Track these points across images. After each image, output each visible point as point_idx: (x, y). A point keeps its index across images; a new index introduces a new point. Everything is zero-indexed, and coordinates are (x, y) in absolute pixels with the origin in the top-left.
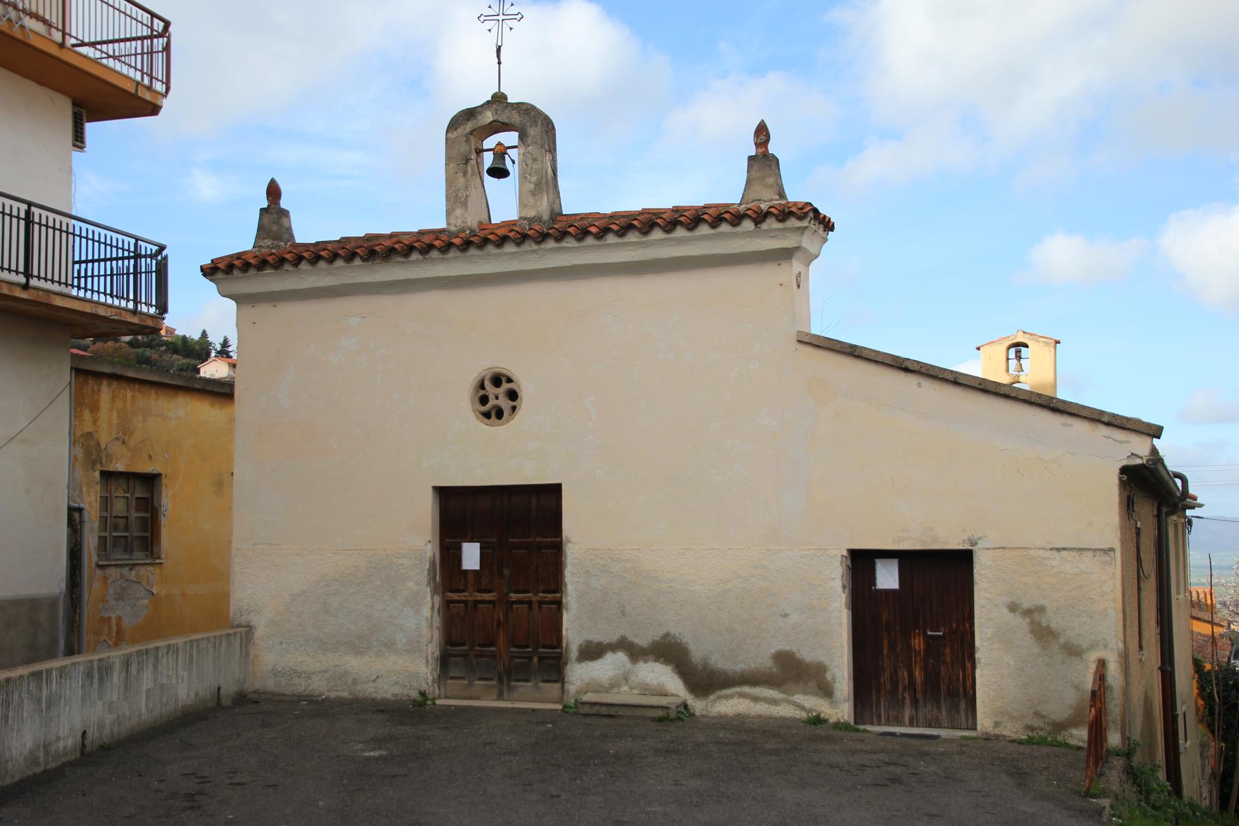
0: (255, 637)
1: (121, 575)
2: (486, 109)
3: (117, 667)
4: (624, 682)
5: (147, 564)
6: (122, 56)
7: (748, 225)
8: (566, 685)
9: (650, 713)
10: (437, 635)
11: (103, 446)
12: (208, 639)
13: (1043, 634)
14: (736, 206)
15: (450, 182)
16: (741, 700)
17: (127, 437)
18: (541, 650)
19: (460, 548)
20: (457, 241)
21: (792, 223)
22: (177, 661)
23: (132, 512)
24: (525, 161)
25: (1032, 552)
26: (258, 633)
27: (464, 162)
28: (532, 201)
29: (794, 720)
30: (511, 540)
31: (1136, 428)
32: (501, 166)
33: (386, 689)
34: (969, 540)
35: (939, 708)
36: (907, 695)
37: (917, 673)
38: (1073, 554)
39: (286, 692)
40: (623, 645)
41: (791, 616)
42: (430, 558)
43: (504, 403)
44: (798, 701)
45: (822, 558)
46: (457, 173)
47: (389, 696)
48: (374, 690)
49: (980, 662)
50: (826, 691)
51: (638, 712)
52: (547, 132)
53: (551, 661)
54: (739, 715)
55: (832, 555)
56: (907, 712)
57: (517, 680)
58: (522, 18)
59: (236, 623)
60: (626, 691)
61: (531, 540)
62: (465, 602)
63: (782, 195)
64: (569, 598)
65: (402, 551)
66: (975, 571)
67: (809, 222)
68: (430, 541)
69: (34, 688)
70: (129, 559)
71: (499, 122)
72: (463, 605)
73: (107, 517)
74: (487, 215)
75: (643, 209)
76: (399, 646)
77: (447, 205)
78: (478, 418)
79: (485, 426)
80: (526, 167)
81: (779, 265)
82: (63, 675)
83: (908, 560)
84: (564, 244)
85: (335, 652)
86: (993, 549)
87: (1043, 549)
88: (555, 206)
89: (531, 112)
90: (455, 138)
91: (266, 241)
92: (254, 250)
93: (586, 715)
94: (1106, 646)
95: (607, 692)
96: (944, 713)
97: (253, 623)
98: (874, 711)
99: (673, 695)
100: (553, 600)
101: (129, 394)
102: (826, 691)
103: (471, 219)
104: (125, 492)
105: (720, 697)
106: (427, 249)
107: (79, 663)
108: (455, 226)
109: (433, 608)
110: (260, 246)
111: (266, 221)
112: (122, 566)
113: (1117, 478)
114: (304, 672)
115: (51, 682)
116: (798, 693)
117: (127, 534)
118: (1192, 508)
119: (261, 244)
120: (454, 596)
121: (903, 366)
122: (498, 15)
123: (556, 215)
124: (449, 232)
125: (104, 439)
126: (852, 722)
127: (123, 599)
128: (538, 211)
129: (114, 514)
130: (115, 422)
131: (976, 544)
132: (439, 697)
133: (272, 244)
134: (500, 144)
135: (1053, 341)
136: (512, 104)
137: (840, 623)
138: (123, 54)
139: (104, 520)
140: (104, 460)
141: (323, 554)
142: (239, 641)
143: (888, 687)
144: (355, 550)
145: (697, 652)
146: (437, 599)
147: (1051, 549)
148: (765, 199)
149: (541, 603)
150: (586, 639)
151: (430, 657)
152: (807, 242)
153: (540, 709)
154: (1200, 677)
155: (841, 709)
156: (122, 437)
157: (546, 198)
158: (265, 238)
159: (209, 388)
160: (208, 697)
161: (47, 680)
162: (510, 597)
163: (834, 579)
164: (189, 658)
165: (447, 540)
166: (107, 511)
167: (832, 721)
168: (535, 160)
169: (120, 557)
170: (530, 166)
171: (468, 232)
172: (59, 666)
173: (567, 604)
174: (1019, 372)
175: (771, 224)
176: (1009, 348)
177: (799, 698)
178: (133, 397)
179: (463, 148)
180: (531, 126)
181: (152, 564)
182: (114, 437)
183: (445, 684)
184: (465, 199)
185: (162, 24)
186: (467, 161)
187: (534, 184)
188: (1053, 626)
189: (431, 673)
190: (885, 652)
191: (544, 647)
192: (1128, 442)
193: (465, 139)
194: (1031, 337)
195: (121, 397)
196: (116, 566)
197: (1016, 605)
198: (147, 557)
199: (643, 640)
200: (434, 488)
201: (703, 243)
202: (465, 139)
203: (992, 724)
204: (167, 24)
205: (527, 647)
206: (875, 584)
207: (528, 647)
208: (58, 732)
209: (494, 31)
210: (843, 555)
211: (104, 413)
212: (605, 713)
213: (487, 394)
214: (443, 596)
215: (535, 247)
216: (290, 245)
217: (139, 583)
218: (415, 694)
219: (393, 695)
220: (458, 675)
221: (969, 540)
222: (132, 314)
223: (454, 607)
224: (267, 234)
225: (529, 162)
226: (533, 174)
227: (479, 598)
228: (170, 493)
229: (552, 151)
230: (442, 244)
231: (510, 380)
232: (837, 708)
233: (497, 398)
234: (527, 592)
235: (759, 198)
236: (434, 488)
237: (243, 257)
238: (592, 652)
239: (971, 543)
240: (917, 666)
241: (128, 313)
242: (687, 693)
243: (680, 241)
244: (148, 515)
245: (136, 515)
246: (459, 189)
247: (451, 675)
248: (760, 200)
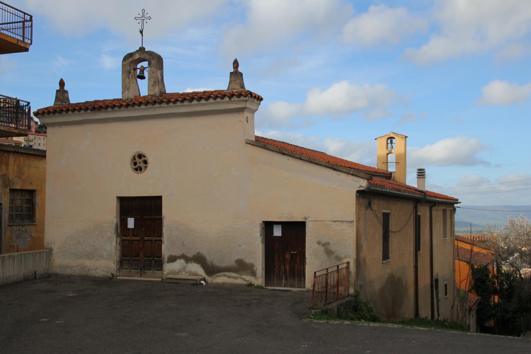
0: (53, 253)
4: (183, 270)
5: (30, 225)
6: (8, 29)
7: (227, 99)
9: (191, 282)
10: (118, 253)
11: (11, 179)
12: (30, 253)
13: (329, 252)
14: (225, 91)
15: (123, 81)
16: (224, 277)
18: (155, 258)
19: (127, 220)
20: (124, 104)
21: (242, 98)
22: (14, 261)
23: (24, 205)
24: (150, 73)
25: (326, 222)
26: (54, 252)
29: (242, 285)
30: (145, 217)
31: (361, 176)
32: (143, 75)
33: (100, 273)
34: (304, 218)
35: (295, 280)
36: (283, 275)
37: (287, 267)
38: (340, 223)
39: (64, 274)
41: (242, 246)
42: (115, 223)
43: (142, 165)
44: (244, 278)
46: (126, 77)
47: (101, 275)
48: (95, 273)
49: (307, 263)
50: (254, 274)
51: (186, 282)
52: (158, 62)
54: (223, 283)
56: (284, 282)
58: (135, 18)
59: (46, 248)
60: (184, 274)
62: (129, 240)
63: (242, 86)
64: (164, 239)
66: (306, 229)
67: (249, 98)
70: (22, 223)
72: (128, 241)
73: (13, 207)
74: (139, 93)
75: (193, 92)
77: (122, 90)
78: (133, 171)
79: (135, 174)
81: (239, 114)
83: (285, 225)
84: (162, 105)
85: (82, 259)
86: (313, 221)
87: (329, 221)
88: (162, 90)
90: (125, 64)
91: (58, 102)
93: (168, 283)
94: (350, 257)
95: (177, 274)
96: (296, 282)
98: (272, 281)
99: (200, 276)
101: (22, 159)
102: (254, 274)
103: (131, 95)
104: (21, 197)
105: (217, 276)
106: (113, 107)
108: (125, 98)
109: (116, 242)
110: (56, 104)
111: (58, 95)
112: (19, 225)
113: (355, 195)
116: (244, 275)
117: (22, 213)
118: (457, 203)
119: (56, 104)
120: (125, 238)
121: (282, 152)
122: (142, 17)
123: (163, 93)
124: (123, 100)
125: (11, 177)
126: (264, 285)
128: (154, 93)
129: (16, 205)
131: (307, 219)
132: (119, 276)
133: (61, 104)
134: (142, 66)
135: (404, 137)
137: (259, 249)
138: (19, 27)
139: (11, 209)
140: (11, 185)
143: (277, 272)
144: (89, 220)
145: (209, 259)
146: (119, 239)
147: (332, 221)
148: (236, 89)
149: (156, 241)
150: (170, 254)
151: (115, 261)
152: (248, 105)
153: (153, 281)
154: (473, 270)
155: (259, 280)
158: (58, 101)
162: (145, 239)
163: (258, 232)
165: (123, 217)
166: (13, 204)
167: (256, 285)
168: (154, 73)
169: (19, 222)
170: (152, 75)
171: (129, 100)
174: (392, 149)
175: (235, 98)
176: (388, 139)
177: (244, 277)
179: (128, 68)
181: (32, 225)
182: (15, 175)
184: (129, 88)
185: (30, 17)
186: (130, 73)
187: (153, 82)
188: (332, 250)
190: (276, 259)
192: (359, 181)
193: (129, 64)
194: (396, 135)
197: (320, 242)
199: (190, 255)
201: (211, 106)
203: (311, 286)
204: (31, 17)
205: (150, 257)
206: (273, 234)
209: (141, 23)
210: (260, 224)
211: (11, 166)
212: (175, 282)
215: (152, 106)
216: (67, 104)
218: (110, 275)
219: (102, 275)
220: (126, 267)
221: (304, 218)
222: (15, 129)
223: (125, 242)
225: (152, 74)
226: (153, 78)
227: (134, 239)
229: (161, 69)
231: (144, 157)
232: (257, 280)
233: (140, 163)
234: (150, 236)
235: (234, 88)
236: (118, 197)
238: (172, 259)
239: (305, 219)
240: (287, 265)
242: (205, 275)
243: (203, 105)
244: (31, 206)
245: (26, 206)
246: (127, 84)
247: (124, 268)
248: (234, 89)
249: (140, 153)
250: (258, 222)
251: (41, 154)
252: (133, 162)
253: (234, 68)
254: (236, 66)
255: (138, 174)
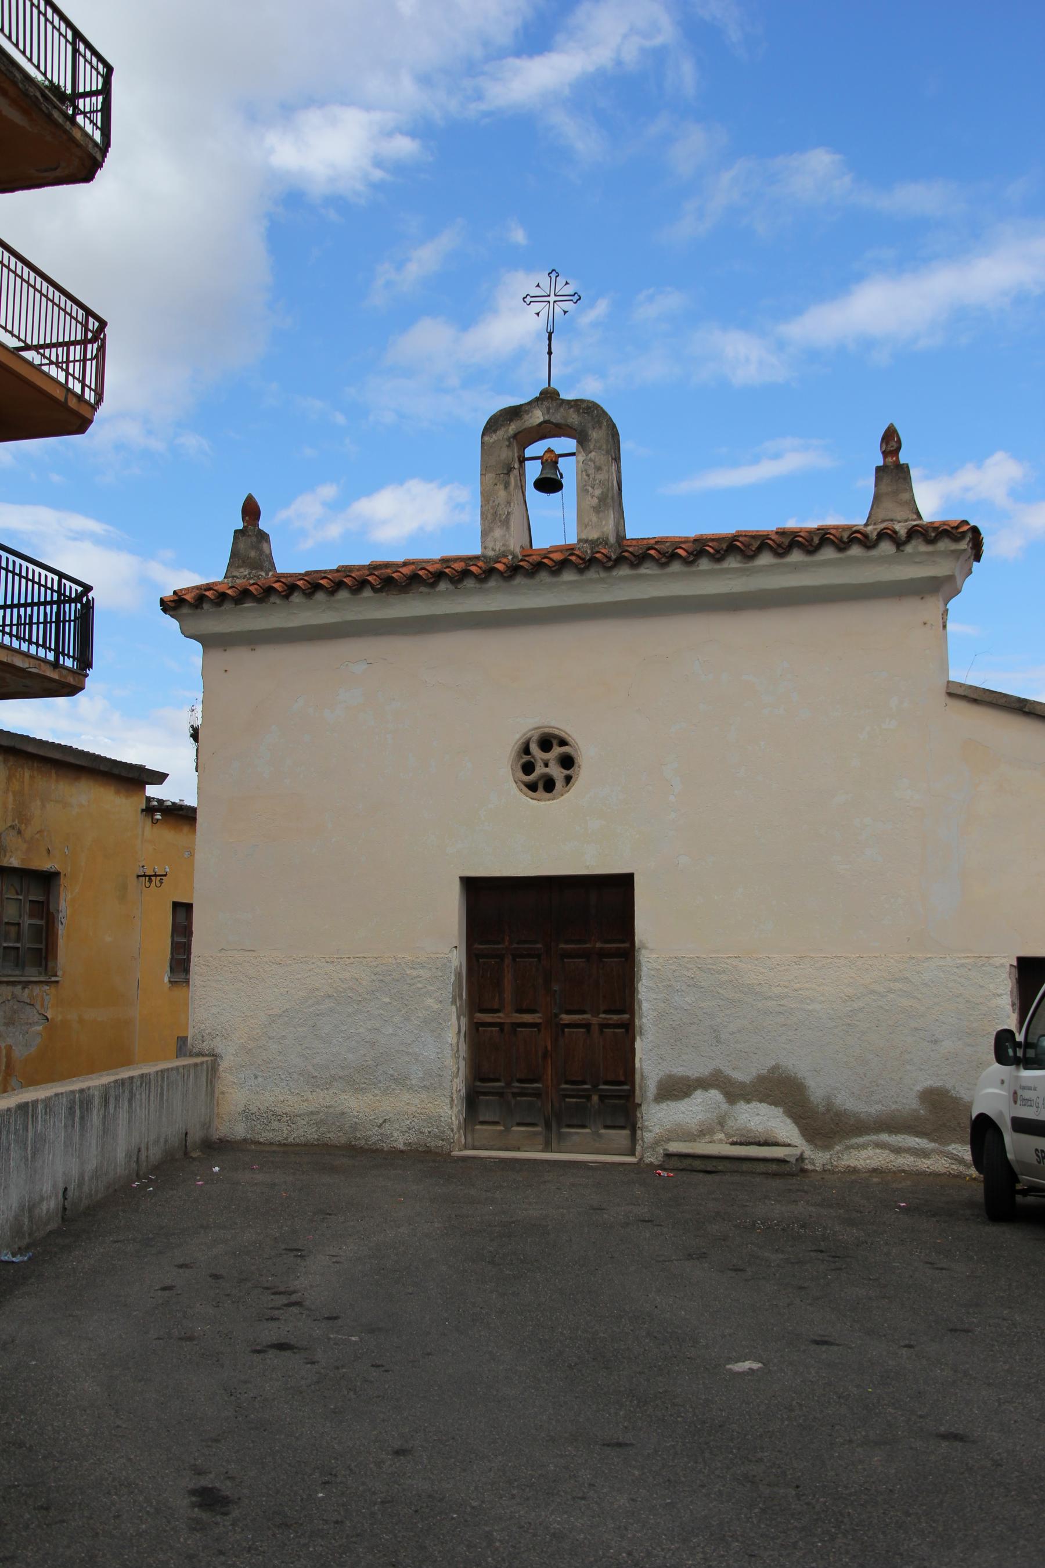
0: (221, 1069)
1: (13, 994)
2: (535, 407)
3: (96, 1102)
4: (719, 1128)
8: (639, 1132)
9: (761, 1167)
17: (23, 825)
22: (149, 1097)
24: (586, 470)
26: (224, 1065)
27: (505, 472)
28: (594, 519)
39: (261, 1140)
40: (716, 1081)
41: (943, 1043)
44: (954, 1152)
45: (984, 968)
53: (616, 1101)
55: (997, 964)
57: (569, 1126)
58: (580, 299)
60: (721, 1140)
61: (588, 945)
62: (500, 1025)
64: (644, 1020)
65: (419, 961)
68: (456, 947)
69: (21, 1126)
70: (22, 976)
71: (552, 423)
74: (528, 540)
75: (738, 532)
76: (413, 1082)
78: (521, 790)
80: (586, 478)
82: (48, 1110)
84: (643, 571)
89: (593, 411)
90: (493, 443)
91: (242, 570)
92: (226, 580)
97: (218, 1051)
100: (619, 1022)
101: (27, 774)
103: (515, 544)
105: (848, 1148)
107: (62, 1093)
110: (233, 577)
111: (241, 546)
114: (286, 1114)
115: (37, 1118)
116: (953, 1142)
117: (19, 945)
119: (235, 573)
120: (487, 1018)
122: (549, 296)
127: (14, 1024)
130: (10, 807)
133: (249, 574)
134: (550, 451)
136: (568, 402)
141: (313, 963)
142: (205, 1073)
144: (354, 958)
145: (818, 1089)
146: (464, 1020)
148: (899, 519)
156: (18, 825)
157: (612, 516)
158: (239, 567)
159: (116, 771)
160: (176, 1145)
161: (33, 1116)
162: (561, 1019)
163: (1001, 995)
164: (160, 1094)
165: (476, 946)
168: (598, 469)
169: (10, 972)
170: (592, 476)
172: (43, 1097)
173: (640, 1027)
178: (32, 777)
180: (594, 428)
181: (47, 983)
183: (473, 1130)
185: (97, 324)
189: (456, 1117)
191: (606, 1083)
193: (507, 443)
195: (18, 777)
196: (8, 983)
198: (40, 974)
199: (743, 1074)
200: (461, 879)
202: (507, 443)
204: (103, 324)
207: (584, 1083)
208: (42, 1190)
210: (1011, 965)
213: (532, 760)
214: (471, 1018)
217: (33, 1005)
220: (487, 1118)
224: (244, 562)
225: (591, 471)
228: (69, 897)
230: (479, 571)
231: (563, 743)
233: (546, 765)
234: (584, 1012)
236: (461, 879)
237: (216, 588)
241: (48, 666)
243: (796, 568)
244: (42, 922)
247: (481, 1119)
248: (892, 520)
249: (546, 730)
250: (1004, 961)
251: (78, 762)
252: (519, 761)
253: (885, 454)
254: (894, 448)
255: (542, 803)
